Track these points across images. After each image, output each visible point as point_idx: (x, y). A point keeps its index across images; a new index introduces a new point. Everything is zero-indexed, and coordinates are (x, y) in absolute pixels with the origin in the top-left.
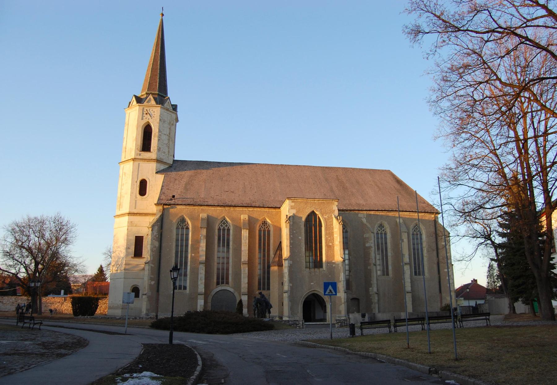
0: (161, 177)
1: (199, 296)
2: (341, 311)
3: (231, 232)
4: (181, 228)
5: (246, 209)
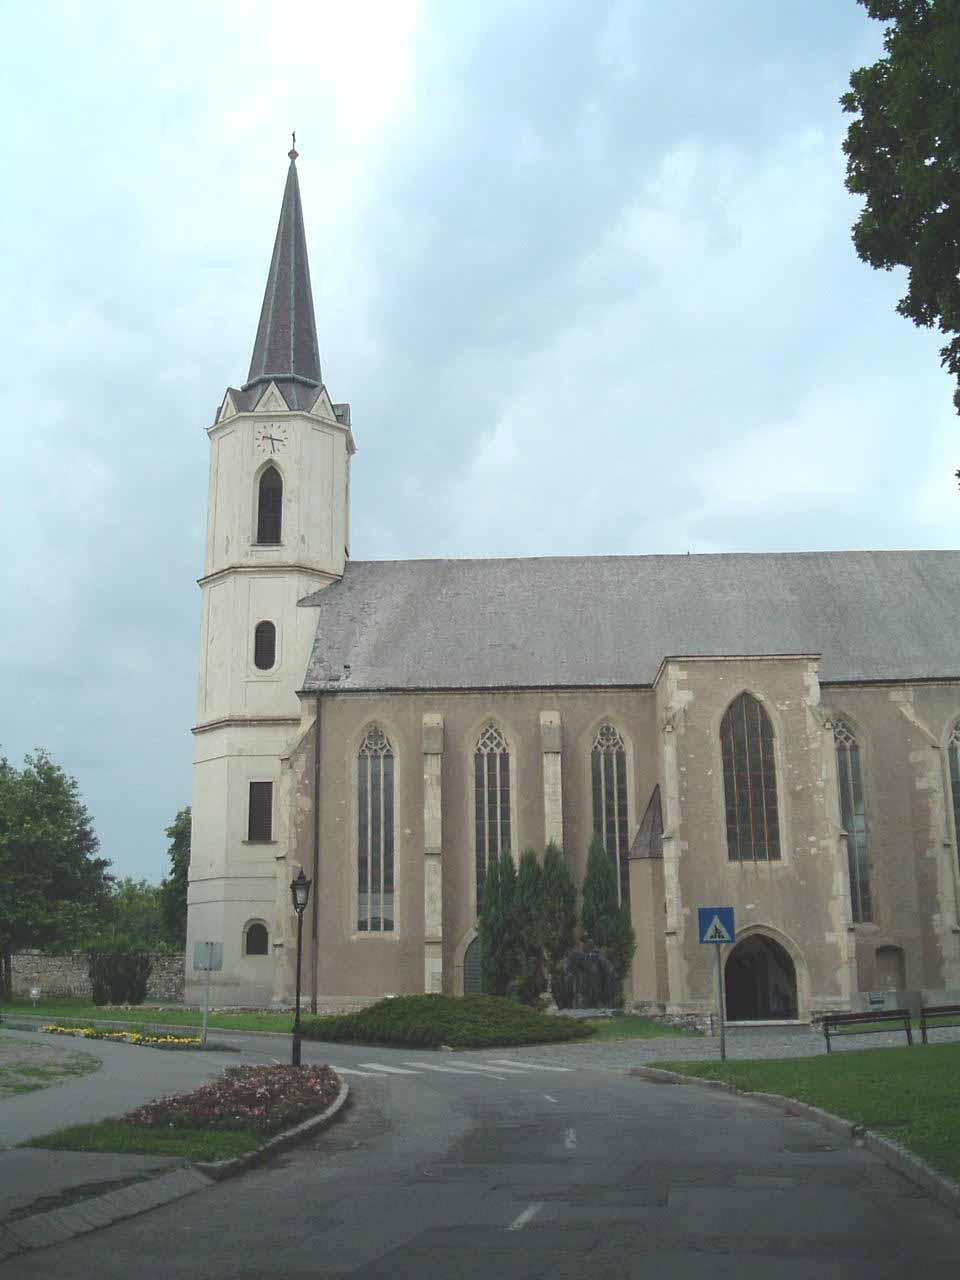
0: (310, 615)
1: (428, 949)
3: (630, 760)
4: (372, 757)
5: (553, 695)
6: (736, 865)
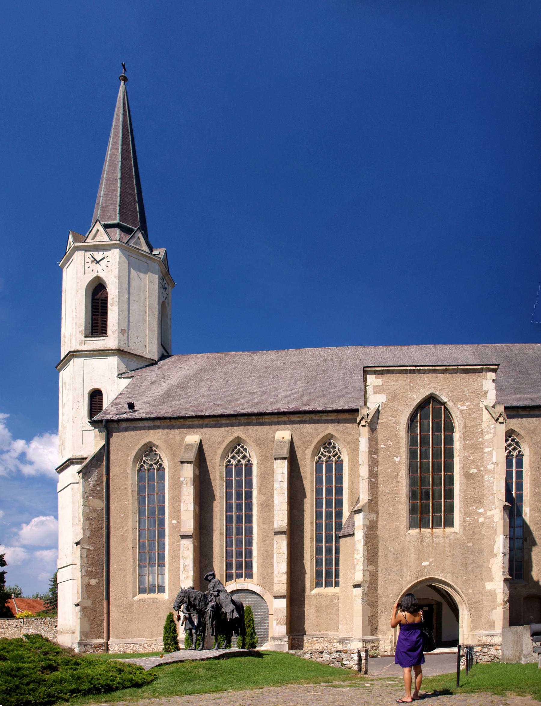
2: (494, 623)
6: (414, 532)
